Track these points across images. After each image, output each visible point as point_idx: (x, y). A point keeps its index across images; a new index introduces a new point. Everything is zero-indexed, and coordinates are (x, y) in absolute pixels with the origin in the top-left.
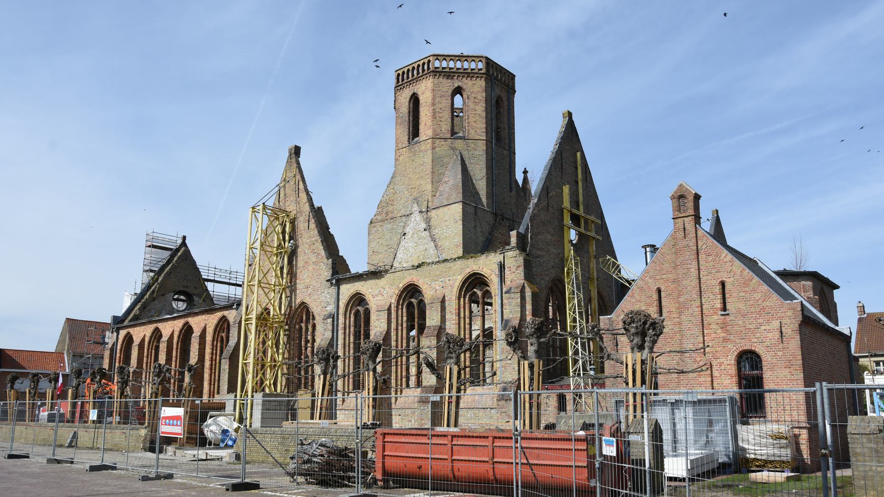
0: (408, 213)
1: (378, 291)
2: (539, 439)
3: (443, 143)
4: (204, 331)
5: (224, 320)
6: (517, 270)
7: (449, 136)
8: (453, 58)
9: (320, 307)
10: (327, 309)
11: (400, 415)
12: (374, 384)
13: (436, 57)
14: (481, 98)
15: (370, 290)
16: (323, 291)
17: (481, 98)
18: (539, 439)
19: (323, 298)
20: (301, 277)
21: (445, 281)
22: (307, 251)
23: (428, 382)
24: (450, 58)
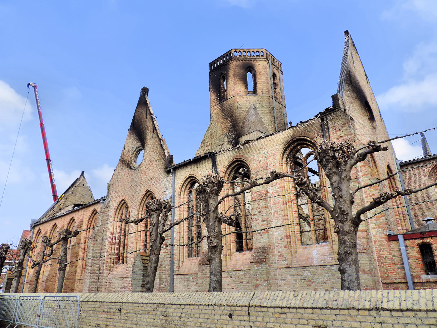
0: (221, 144)
1: (207, 172)
2: (93, 302)
3: (242, 99)
4: (82, 221)
5: (95, 212)
6: (342, 127)
7: (244, 94)
8: (245, 50)
9: (161, 192)
10: (166, 193)
11: (231, 277)
12: (254, 82)
13: (234, 50)
14: (264, 72)
15: (200, 173)
16: (163, 180)
17: (264, 72)
18: (93, 302)
19: (163, 185)
20: (147, 172)
21: (267, 152)
22: (151, 154)
23: (260, 242)
24: (243, 50)
